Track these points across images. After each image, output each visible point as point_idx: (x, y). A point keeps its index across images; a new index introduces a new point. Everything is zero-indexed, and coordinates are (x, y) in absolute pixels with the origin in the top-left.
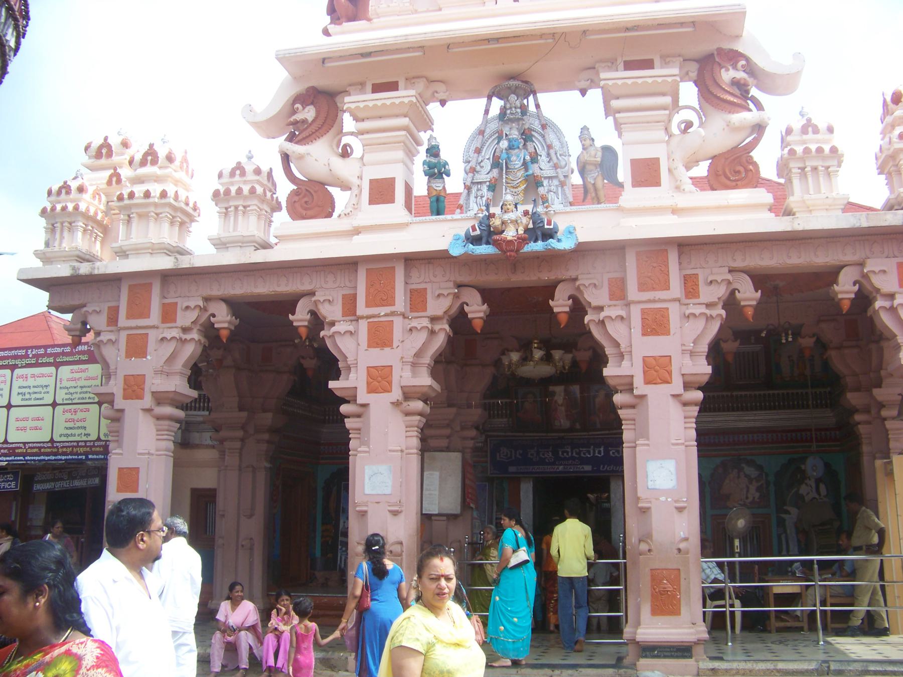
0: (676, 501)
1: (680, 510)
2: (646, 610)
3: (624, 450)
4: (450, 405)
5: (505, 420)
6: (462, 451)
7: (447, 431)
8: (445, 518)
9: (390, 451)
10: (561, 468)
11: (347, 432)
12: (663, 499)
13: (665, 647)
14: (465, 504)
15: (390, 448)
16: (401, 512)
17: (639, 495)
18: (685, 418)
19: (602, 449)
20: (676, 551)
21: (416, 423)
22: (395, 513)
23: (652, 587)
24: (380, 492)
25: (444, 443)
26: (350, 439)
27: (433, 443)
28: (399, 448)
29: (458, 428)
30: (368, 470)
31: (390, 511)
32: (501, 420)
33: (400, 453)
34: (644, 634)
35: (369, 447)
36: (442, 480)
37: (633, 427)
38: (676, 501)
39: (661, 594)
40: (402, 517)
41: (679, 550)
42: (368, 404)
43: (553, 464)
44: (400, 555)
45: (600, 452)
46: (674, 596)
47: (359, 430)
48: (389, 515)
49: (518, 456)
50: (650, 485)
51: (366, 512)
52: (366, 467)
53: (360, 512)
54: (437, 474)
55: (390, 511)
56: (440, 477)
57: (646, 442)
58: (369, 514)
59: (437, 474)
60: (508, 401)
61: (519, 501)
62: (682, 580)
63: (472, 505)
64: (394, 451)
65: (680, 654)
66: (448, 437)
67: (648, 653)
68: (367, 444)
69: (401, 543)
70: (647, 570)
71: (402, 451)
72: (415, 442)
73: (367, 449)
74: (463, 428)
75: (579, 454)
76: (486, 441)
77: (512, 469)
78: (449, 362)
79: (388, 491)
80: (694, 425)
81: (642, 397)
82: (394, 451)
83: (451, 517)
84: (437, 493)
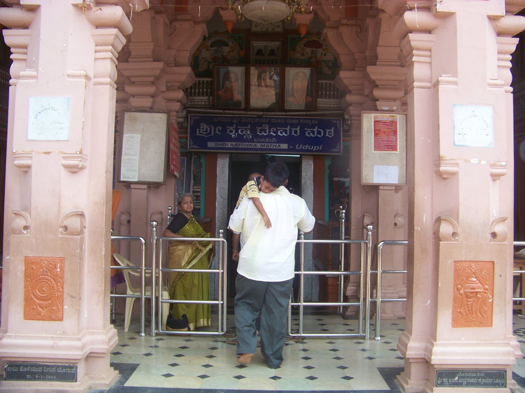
0: (492, 166)
1: (495, 177)
2: (445, 318)
3: (416, 91)
4: (156, 60)
5: (206, 98)
6: (168, 112)
7: (152, 90)
8: (145, 187)
9: (68, 76)
10: (259, 146)
11: (7, 51)
12: (474, 161)
13: (468, 371)
14: (168, 172)
15: (70, 72)
16: (83, 168)
17: (442, 153)
18: (499, 53)
19: (298, 129)
20: (489, 236)
21: (111, 39)
22: (74, 170)
23: (455, 285)
24: (51, 138)
25: (147, 102)
26: (11, 61)
27: (135, 102)
28: (83, 73)
29: (164, 88)
30: (35, 104)
31: (66, 167)
32: (201, 98)
33: (84, 80)
34: (443, 354)
35: (37, 71)
36: (144, 144)
37: (428, 60)
38: (492, 166)
39: (468, 297)
40: (84, 175)
41: (494, 235)
42: (39, 6)
43: (251, 141)
44: (81, 233)
45: (296, 132)
46: (484, 301)
47: (26, 47)
48: (64, 173)
49: (217, 132)
50: (458, 140)
51: (29, 167)
52: (31, 100)
53: (20, 167)
54: (138, 137)
55: (66, 167)
56: (141, 140)
57: (454, 79)
58: (34, 170)
59: (138, 137)
60: (209, 79)
61: (216, 176)
62: (496, 277)
63: (176, 173)
64: (74, 76)
65: (490, 381)
66: (153, 96)
67: (445, 380)
68: (34, 66)
69: (82, 215)
70: (450, 262)
71: (87, 77)
72: (107, 68)
73: (35, 73)
74: (169, 89)
75: (276, 132)
76: (187, 117)
77: (211, 144)
78: (157, 12)
79: (63, 136)
80: (510, 65)
81: (447, 16)
82: (74, 76)
83: (153, 186)
84: (137, 158)
